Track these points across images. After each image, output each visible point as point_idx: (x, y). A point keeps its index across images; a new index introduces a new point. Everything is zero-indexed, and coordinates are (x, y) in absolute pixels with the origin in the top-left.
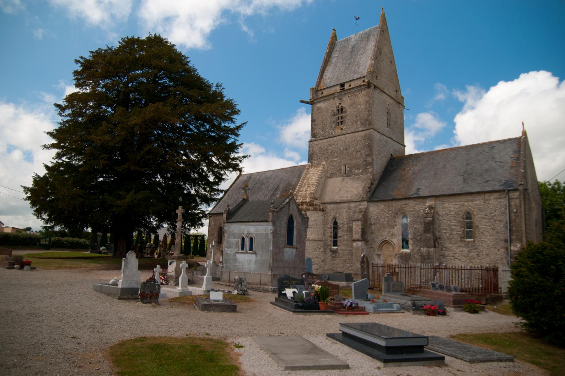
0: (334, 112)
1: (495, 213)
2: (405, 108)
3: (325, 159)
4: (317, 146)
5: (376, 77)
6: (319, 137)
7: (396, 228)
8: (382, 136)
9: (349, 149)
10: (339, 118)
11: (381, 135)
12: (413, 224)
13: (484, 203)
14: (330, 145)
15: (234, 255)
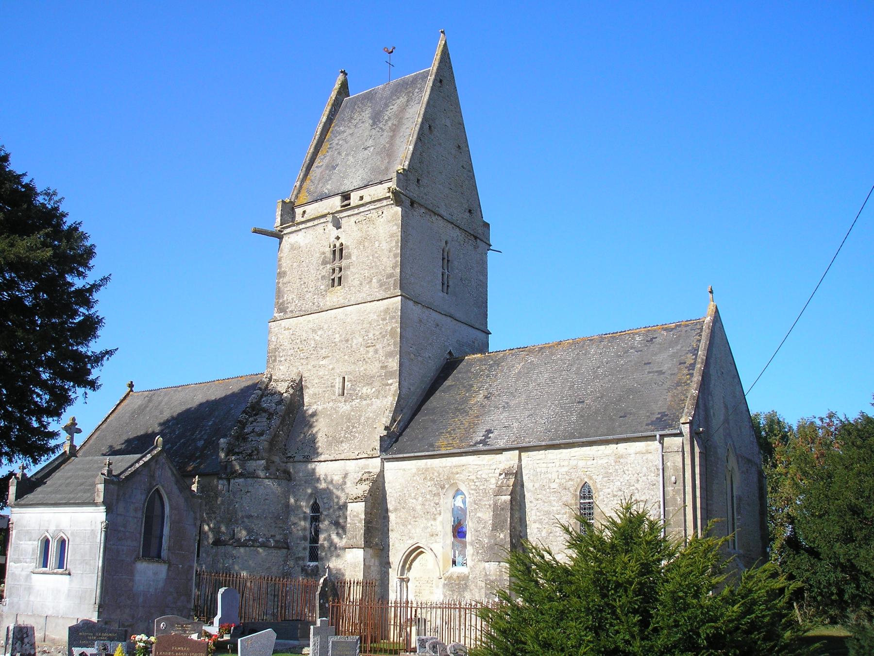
0: (325, 257)
1: (637, 486)
2: (491, 248)
3: (302, 361)
4: (287, 332)
5: (418, 180)
6: (292, 312)
7: (440, 519)
8: (427, 311)
9: (352, 339)
10: (334, 270)
11: (425, 310)
12: (475, 509)
13: (616, 462)
14: (314, 331)
15: (28, 577)
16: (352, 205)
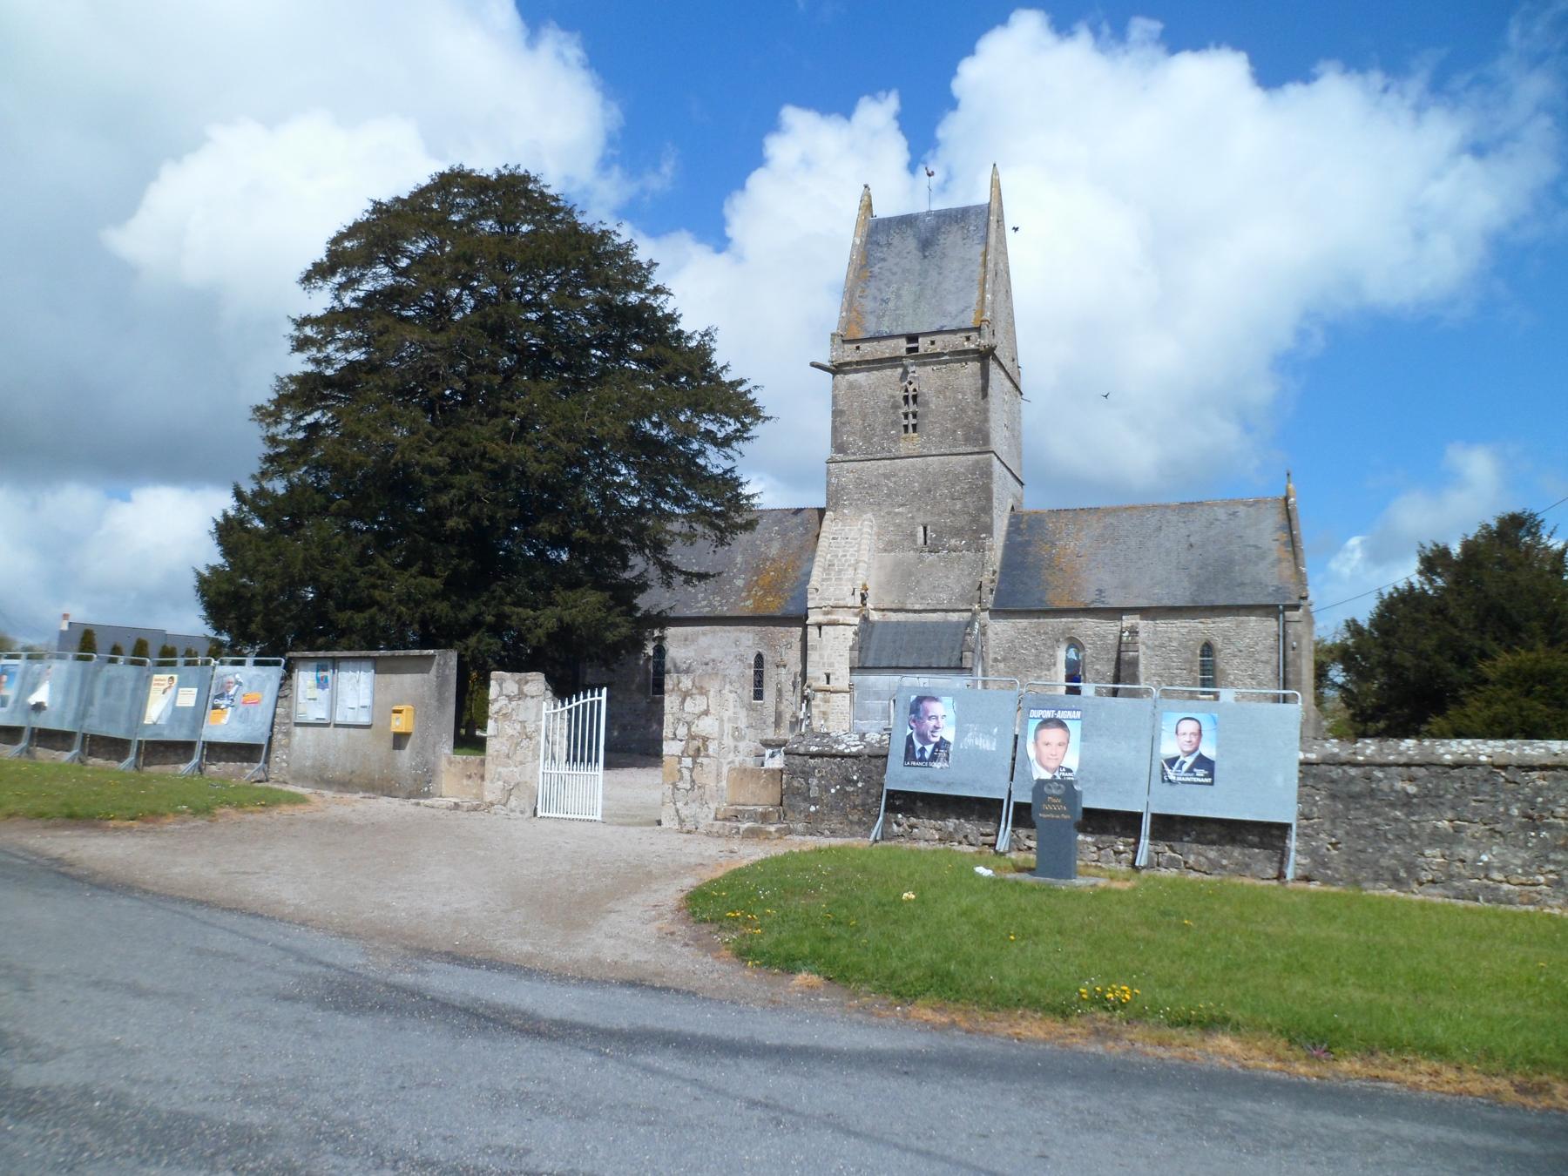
16: (921, 351)
